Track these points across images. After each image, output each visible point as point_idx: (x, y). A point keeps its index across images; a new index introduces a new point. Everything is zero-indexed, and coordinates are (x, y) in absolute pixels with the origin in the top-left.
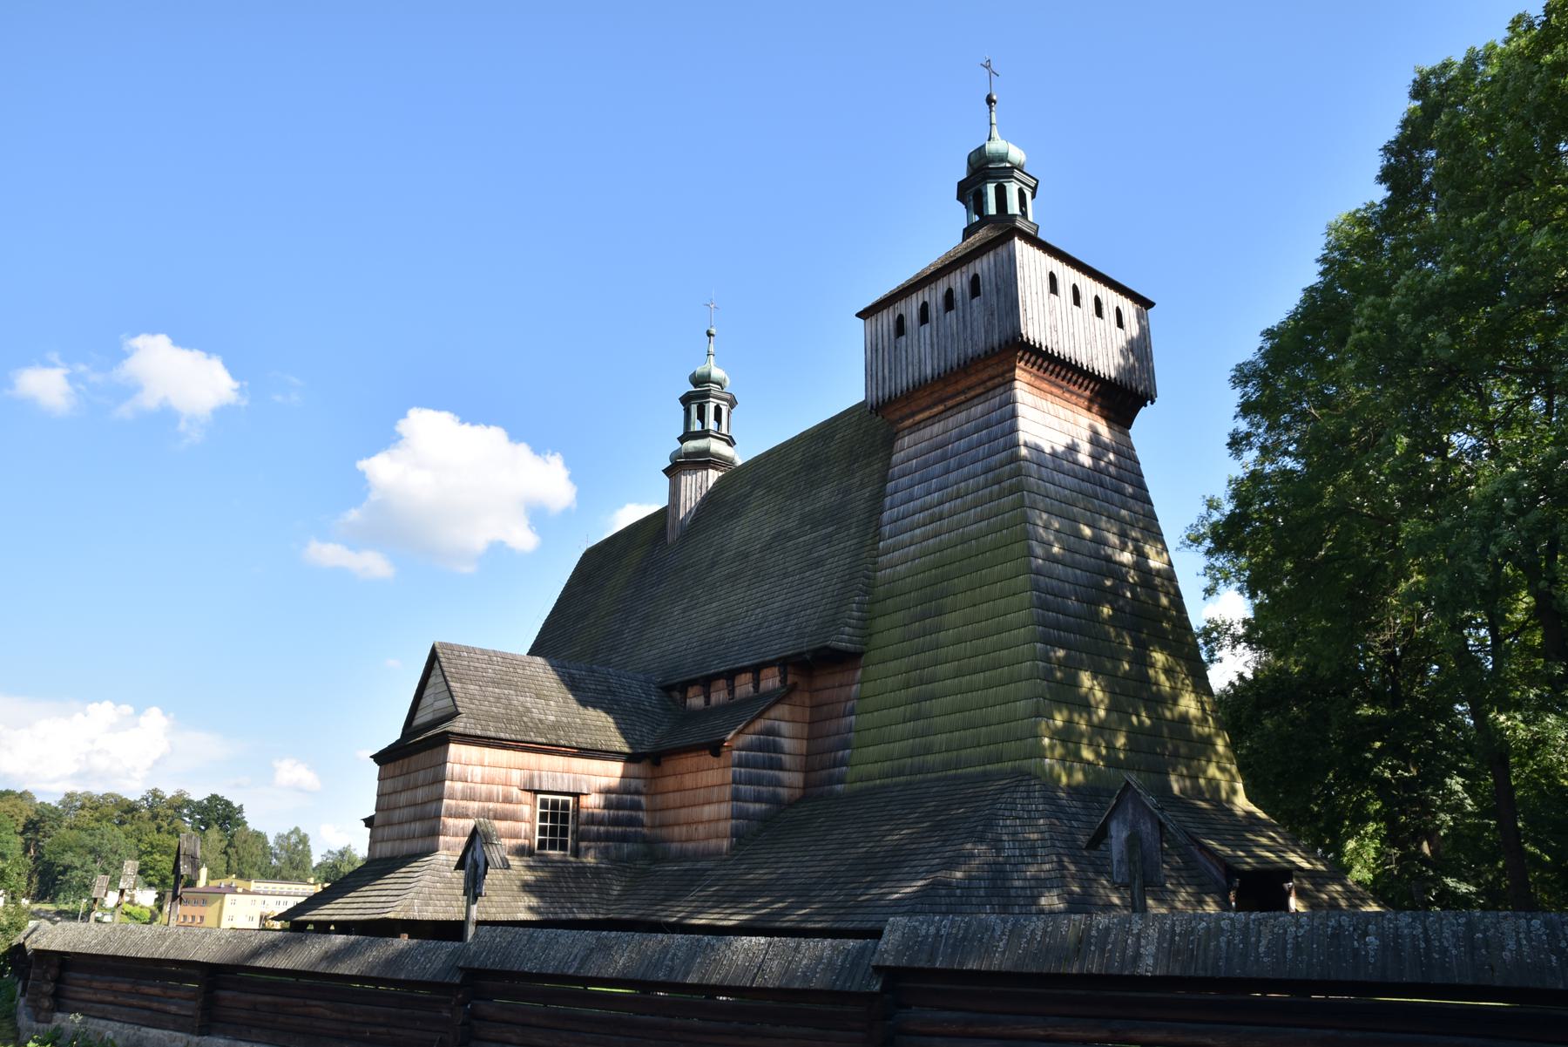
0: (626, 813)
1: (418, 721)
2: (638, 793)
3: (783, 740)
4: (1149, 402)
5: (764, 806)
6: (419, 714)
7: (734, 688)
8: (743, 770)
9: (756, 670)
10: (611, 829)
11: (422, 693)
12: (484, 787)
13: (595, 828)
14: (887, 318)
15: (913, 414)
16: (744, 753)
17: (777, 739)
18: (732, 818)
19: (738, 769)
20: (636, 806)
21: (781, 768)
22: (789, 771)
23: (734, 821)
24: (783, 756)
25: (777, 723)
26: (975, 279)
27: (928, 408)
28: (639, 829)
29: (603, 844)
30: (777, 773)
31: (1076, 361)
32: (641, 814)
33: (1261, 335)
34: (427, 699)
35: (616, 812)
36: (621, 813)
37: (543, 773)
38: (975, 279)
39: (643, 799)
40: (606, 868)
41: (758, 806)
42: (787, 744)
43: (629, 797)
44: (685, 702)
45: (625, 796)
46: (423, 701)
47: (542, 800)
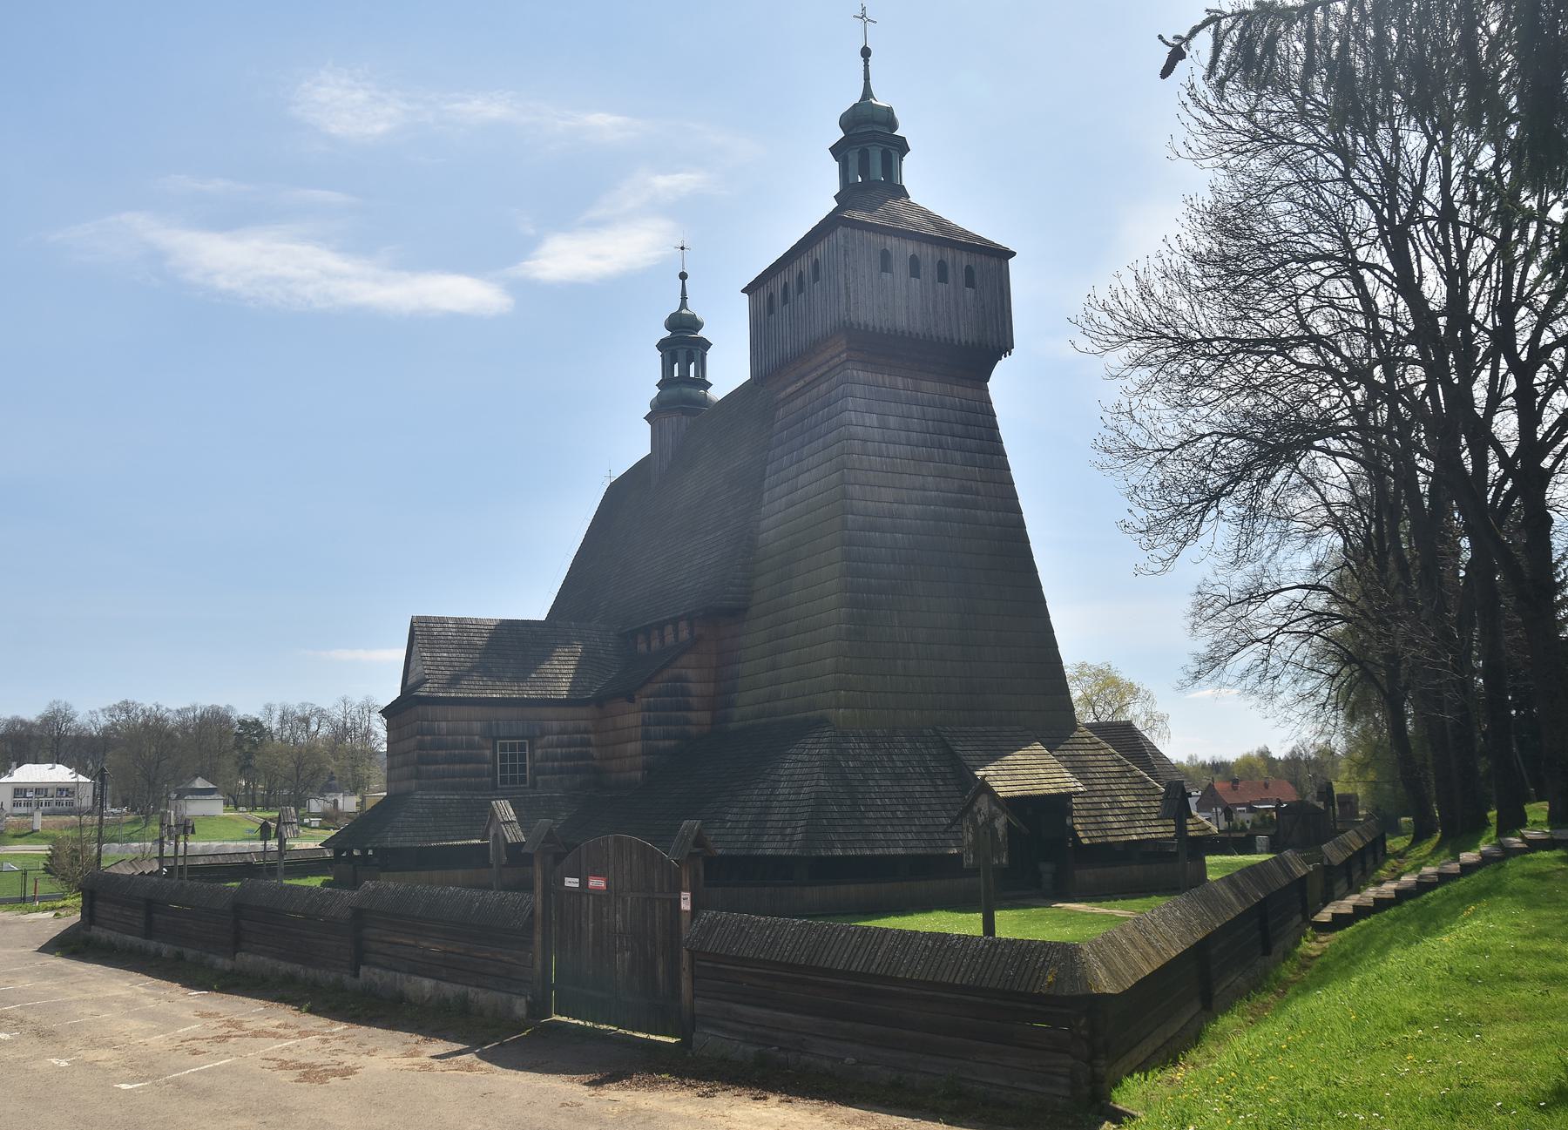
0: (578, 749)
1: (409, 683)
2: (586, 731)
3: (691, 685)
4: (1003, 357)
5: (673, 743)
6: (410, 675)
7: (664, 638)
8: (652, 714)
9: (675, 621)
10: (564, 763)
11: (410, 658)
12: (450, 738)
13: (550, 764)
14: (763, 294)
15: (785, 387)
16: (652, 699)
17: (684, 684)
18: (643, 755)
19: (647, 714)
20: (587, 743)
21: (689, 708)
22: (697, 711)
23: (645, 757)
24: (690, 699)
25: (684, 671)
26: (816, 264)
27: (795, 382)
28: (590, 762)
29: (558, 776)
30: (685, 713)
31: (910, 333)
32: (591, 749)
33: (66, 705)
34: (412, 666)
35: (568, 750)
36: (572, 750)
37: (500, 722)
38: (816, 264)
39: (592, 737)
40: (560, 796)
41: (667, 743)
42: (694, 688)
43: (579, 736)
44: (636, 648)
45: (575, 736)
46: (411, 665)
47: (525, 743)
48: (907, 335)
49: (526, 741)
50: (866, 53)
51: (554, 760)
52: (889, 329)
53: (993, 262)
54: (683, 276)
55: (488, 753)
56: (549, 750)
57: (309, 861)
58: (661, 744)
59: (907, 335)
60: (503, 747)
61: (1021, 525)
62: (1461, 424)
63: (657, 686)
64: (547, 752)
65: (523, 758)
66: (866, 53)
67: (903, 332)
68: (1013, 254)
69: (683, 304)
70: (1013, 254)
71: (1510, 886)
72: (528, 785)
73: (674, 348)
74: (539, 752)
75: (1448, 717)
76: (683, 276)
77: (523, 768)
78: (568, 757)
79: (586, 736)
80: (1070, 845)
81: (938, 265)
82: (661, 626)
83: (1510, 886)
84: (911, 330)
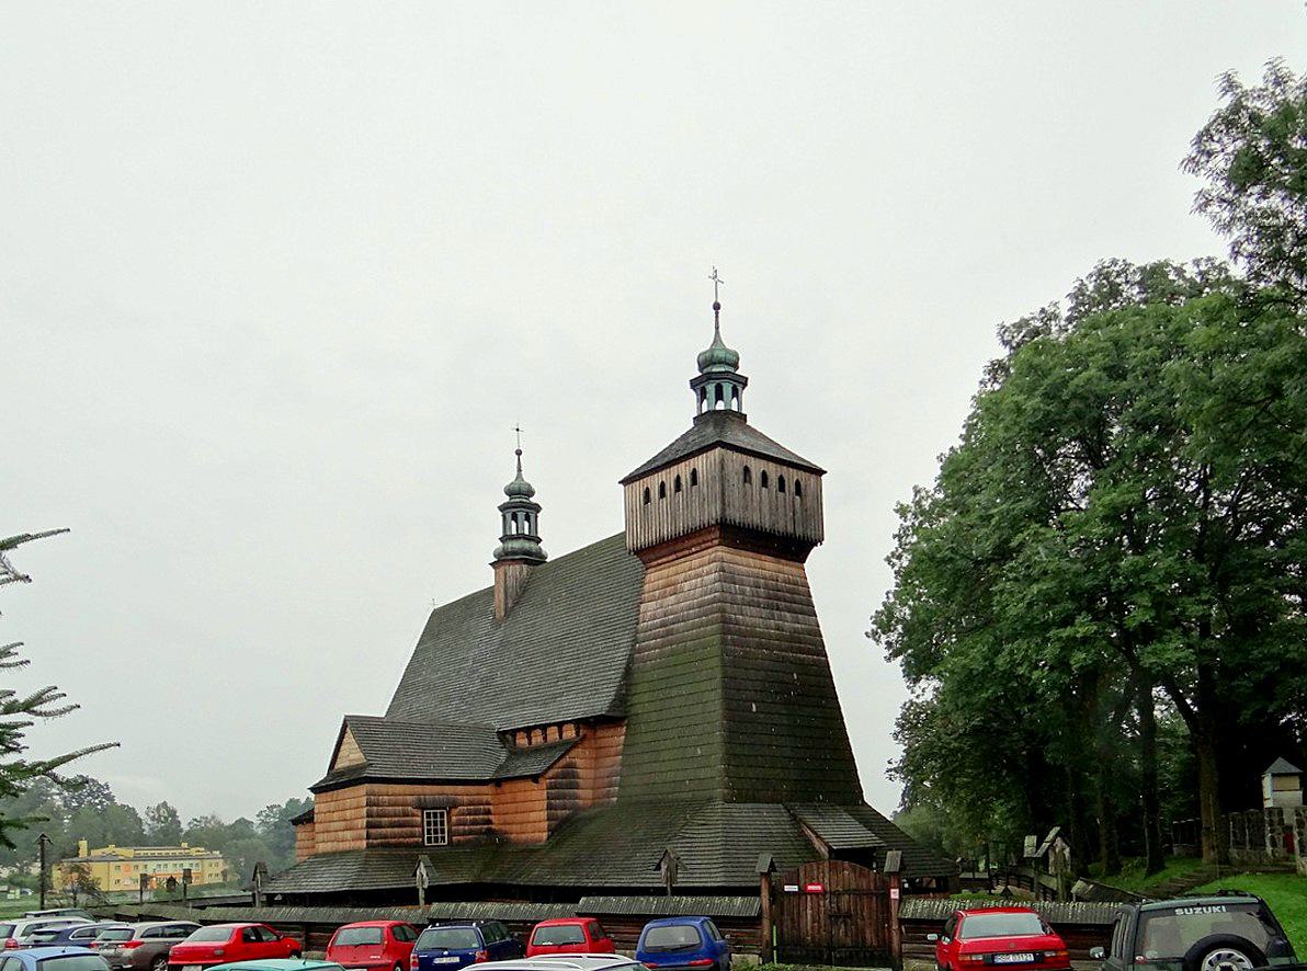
14: (639, 487)
26: (694, 473)
38: (694, 473)
50: (717, 307)
51: (465, 825)
53: (813, 478)
54: (519, 453)
55: (419, 819)
57: (675, 950)
60: (428, 815)
61: (824, 672)
65: (442, 823)
66: (717, 307)
68: (825, 472)
69: (519, 476)
70: (825, 472)
73: (515, 510)
74: (454, 818)
75: (1269, 849)
76: (519, 453)
77: (443, 831)
78: (474, 823)
82: (544, 728)
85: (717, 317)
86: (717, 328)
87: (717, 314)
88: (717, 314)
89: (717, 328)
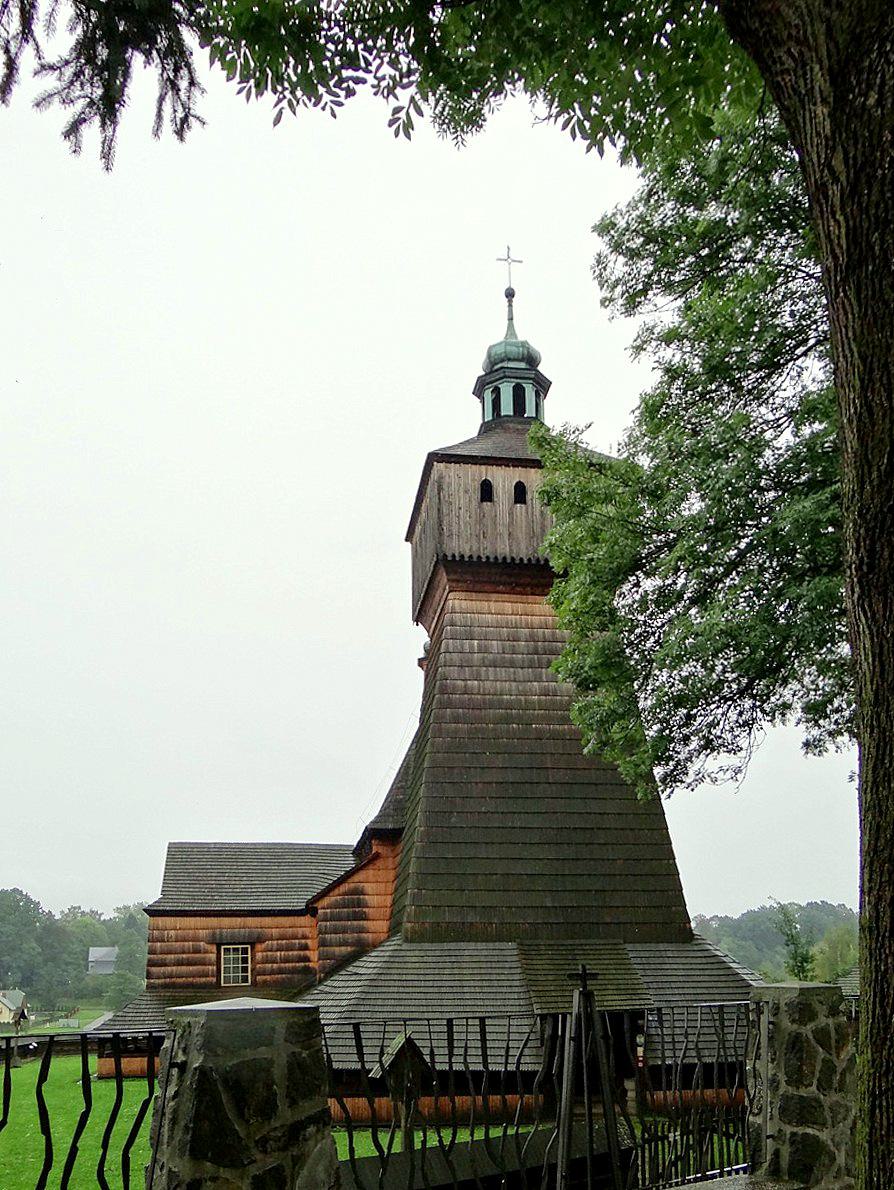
5: (349, 949)
16: (329, 911)
35: (286, 953)
48: (509, 561)
49: (249, 946)
50: (510, 294)
52: (488, 558)
55: (213, 956)
56: (270, 953)
58: (337, 950)
59: (509, 561)
62: (791, 465)
63: (333, 899)
64: (267, 956)
66: (510, 294)
67: (505, 558)
71: (607, 1151)
72: (249, 983)
74: (259, 955)
77: (245, 970)
79: (303, 941)
80: (640, 1065)
81: (482, 485)
83: (607, 1151)
84: (514, 555)
85: (510, 305)
86: (511, 319)
87: (510, 302)
88: (510, 302)
89: (511, 319)
